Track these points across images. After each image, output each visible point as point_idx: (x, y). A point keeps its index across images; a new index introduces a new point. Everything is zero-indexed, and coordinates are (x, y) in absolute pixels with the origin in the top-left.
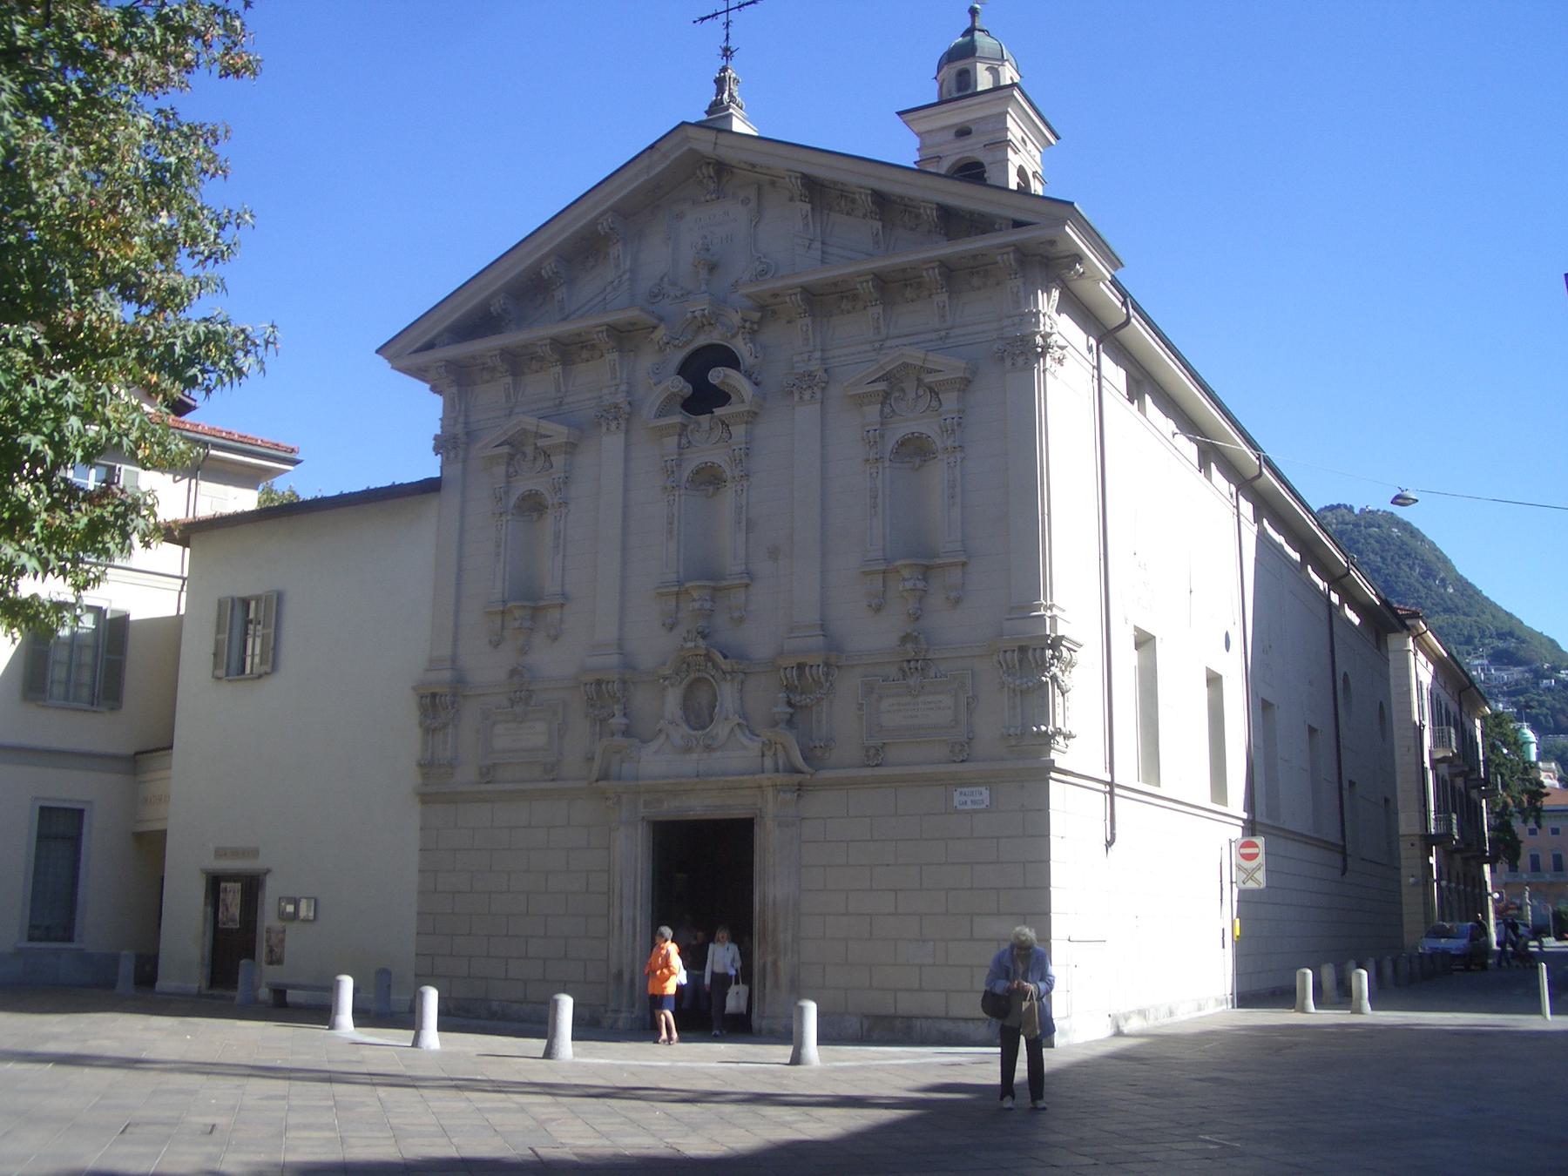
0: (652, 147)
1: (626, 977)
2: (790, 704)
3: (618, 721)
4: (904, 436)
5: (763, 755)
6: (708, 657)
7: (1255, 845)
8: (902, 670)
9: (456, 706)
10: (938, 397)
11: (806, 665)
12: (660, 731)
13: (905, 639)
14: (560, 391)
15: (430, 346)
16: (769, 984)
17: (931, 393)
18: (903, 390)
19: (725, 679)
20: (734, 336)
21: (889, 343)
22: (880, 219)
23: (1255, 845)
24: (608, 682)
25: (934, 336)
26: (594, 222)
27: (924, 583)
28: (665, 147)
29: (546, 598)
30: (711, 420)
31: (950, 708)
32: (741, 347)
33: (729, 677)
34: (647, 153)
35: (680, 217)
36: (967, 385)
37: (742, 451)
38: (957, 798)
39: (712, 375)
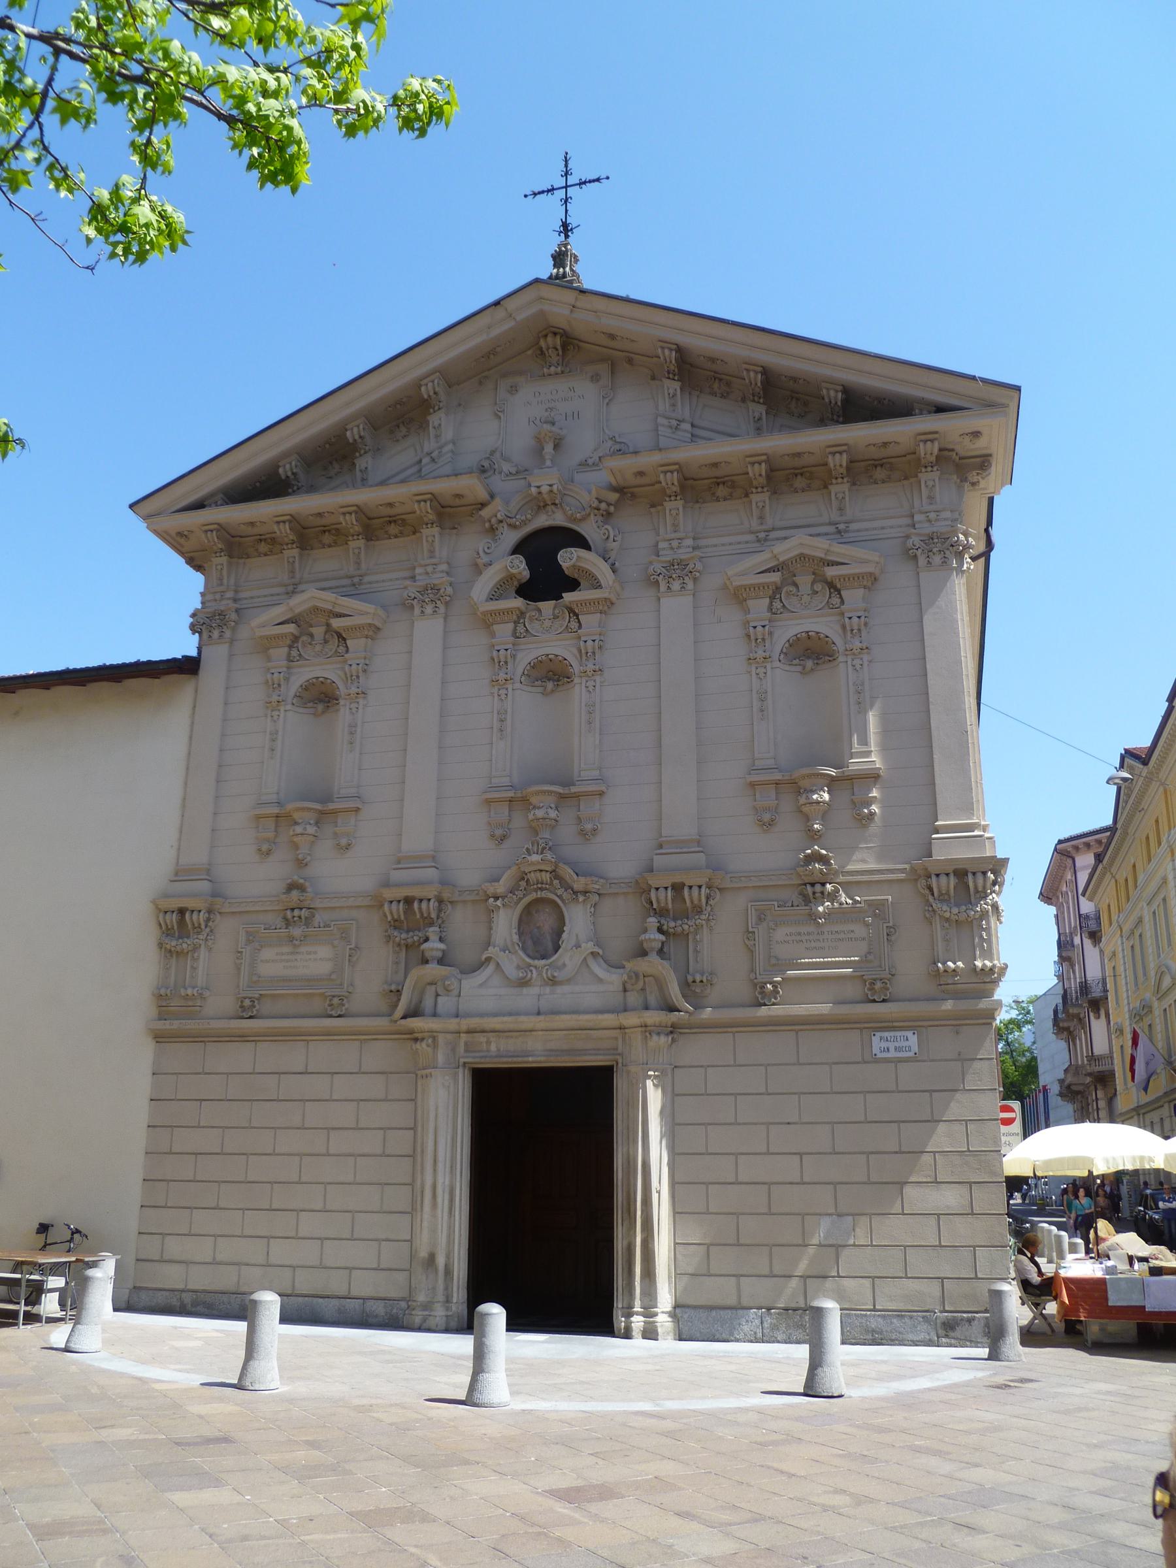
0: (497, 303)
1: (441, 1261)
2: (660, 930)
3: (434, 946)
5: (625, 990)
6: (554, 873)
7: (1012, 1110)
8: (285, 918)
9: (210, 924)
11: (684, 885)
12: (488, 959)
13: (292, 887)
14: (221, 584)
15: (199, 505)
17: (338, 638)
18: (796, 585)
19: (576, 900)
20: (583, 519)
21: (773, 535)
22: (764, 403)
23: (1012, 1110)
24: (421, 901)
25: (751, 537)
26: (417, 384)
28: (510, 305)
29: (336, 800)
30: (554, 608)
31: (864, 939)
32: (588, 530)
33: (581, 898)
34: (490, 309)
35: (514, 389)
37: (509, 651)
38: (877, 1043)
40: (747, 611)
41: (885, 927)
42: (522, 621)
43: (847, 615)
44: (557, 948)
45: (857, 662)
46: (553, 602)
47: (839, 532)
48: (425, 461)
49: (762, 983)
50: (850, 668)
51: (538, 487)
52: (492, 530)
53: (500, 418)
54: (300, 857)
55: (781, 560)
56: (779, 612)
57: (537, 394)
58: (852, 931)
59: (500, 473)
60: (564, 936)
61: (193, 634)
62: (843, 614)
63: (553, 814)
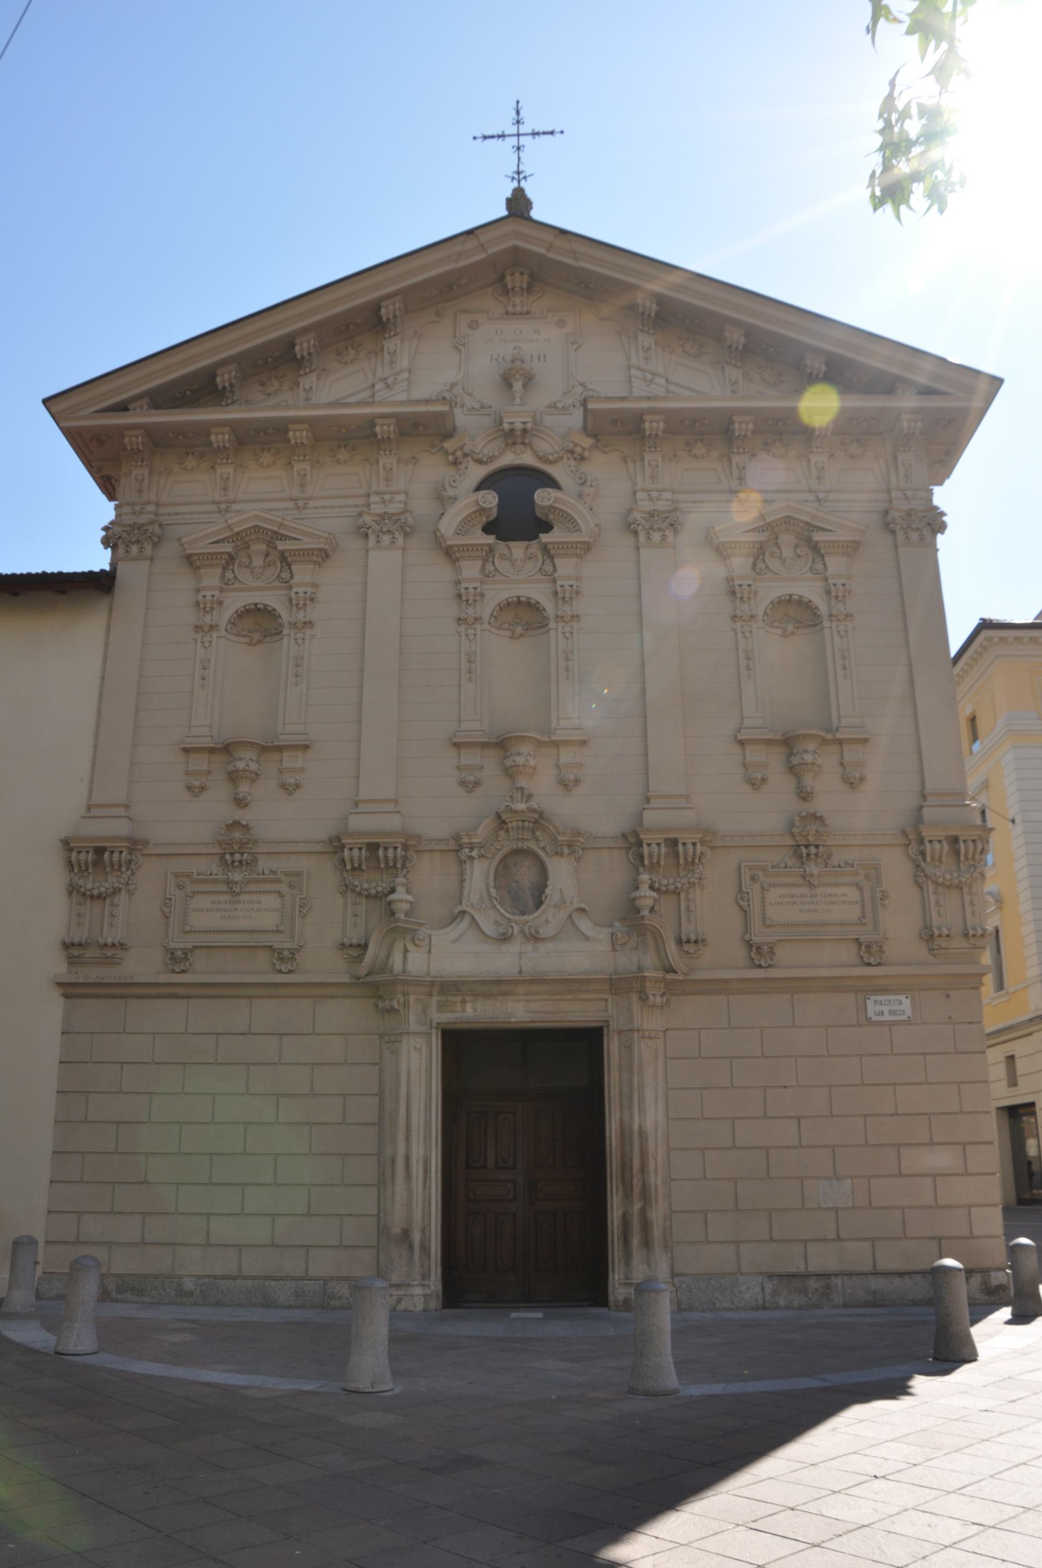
0: (470, 232)
1: (416, 1237)
4: (245, 606)
10: (290, 569)
16: (636, 1240)
21: (312, 503)
27: (257, 766)
28: (484, 237)
34: (463, 238)
35: (473, 325)
36: (324, 560)
39: (538, 495)
40: (458, 570)
41: (298, 900)
42: (231, 567)
43: (559, 583)
44: (539, 903)
45: (300, 635)
46: (525, 543)
47: (819, 500)
48: (378, 387)
49: (280, 949)
50: (835, 634)
51: (511, 423)
52: (455, 463)
53: (460, 351)
54: (241, 796)
55: (768, 520)
56: (762, 573)
57: (499, 333)
58: (845, 895)
59: (463, 406)
60: (548, 891)
61: (106, 548)
62: (555, 581)
63: (254, 767)
